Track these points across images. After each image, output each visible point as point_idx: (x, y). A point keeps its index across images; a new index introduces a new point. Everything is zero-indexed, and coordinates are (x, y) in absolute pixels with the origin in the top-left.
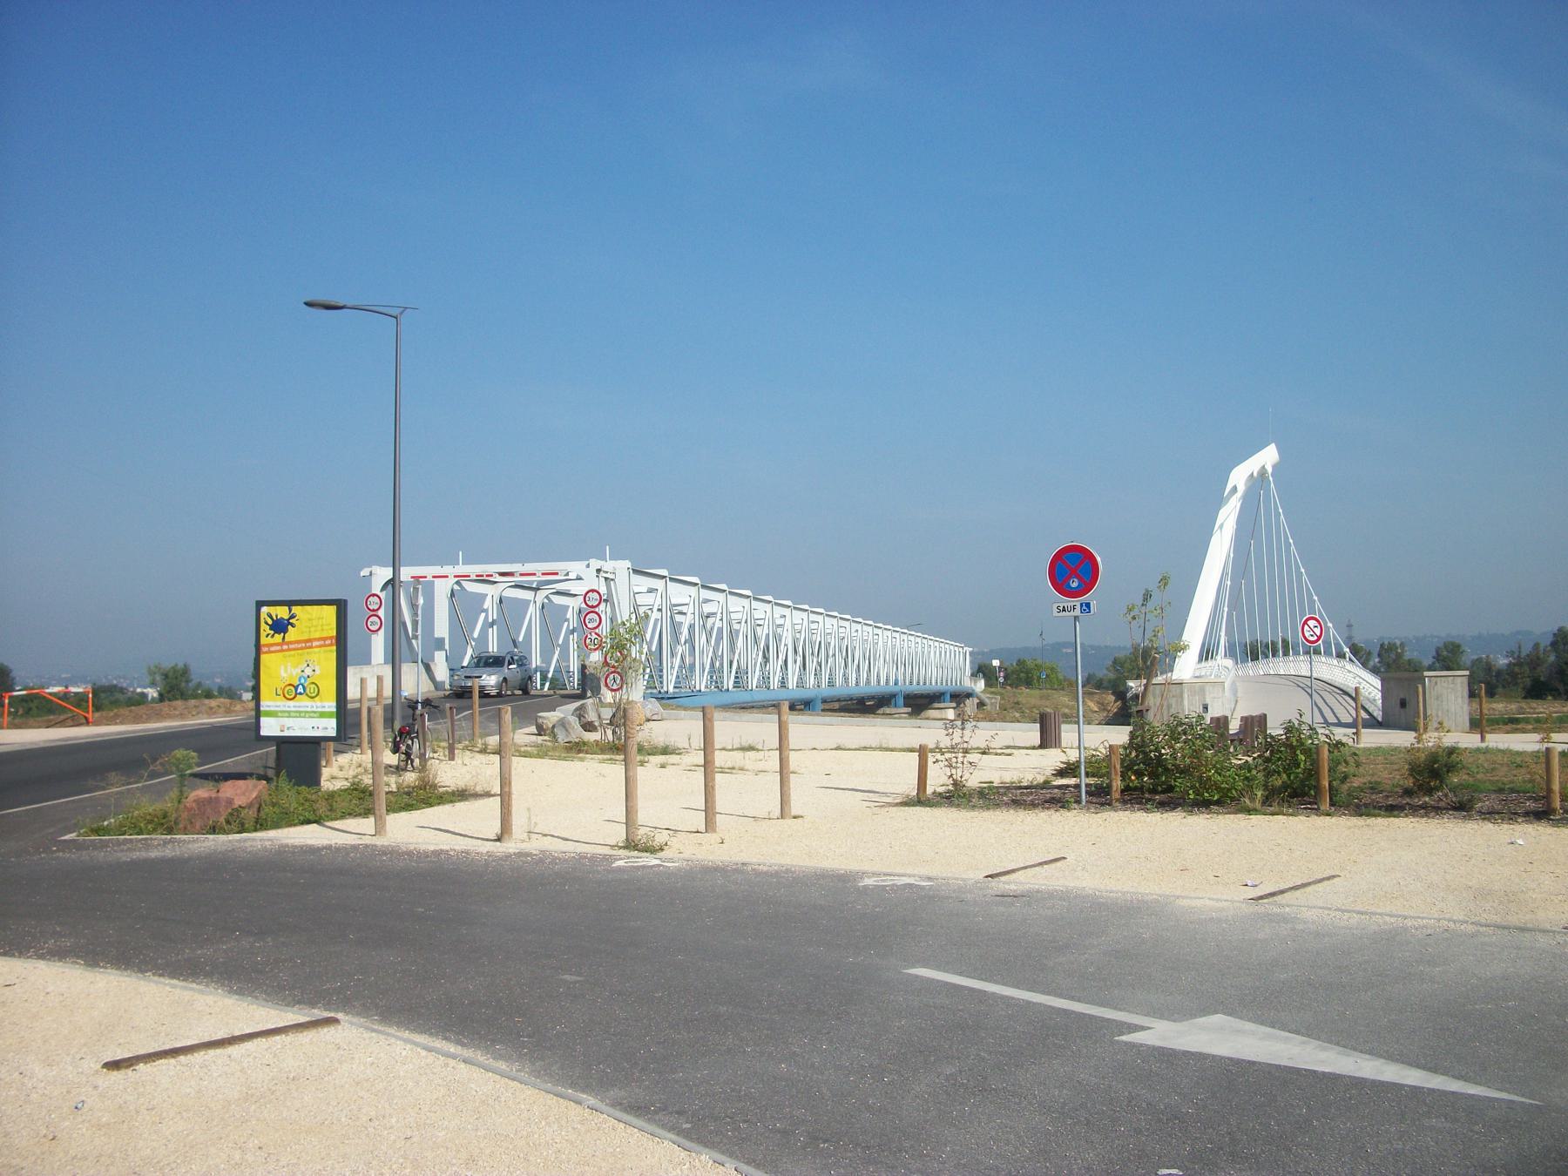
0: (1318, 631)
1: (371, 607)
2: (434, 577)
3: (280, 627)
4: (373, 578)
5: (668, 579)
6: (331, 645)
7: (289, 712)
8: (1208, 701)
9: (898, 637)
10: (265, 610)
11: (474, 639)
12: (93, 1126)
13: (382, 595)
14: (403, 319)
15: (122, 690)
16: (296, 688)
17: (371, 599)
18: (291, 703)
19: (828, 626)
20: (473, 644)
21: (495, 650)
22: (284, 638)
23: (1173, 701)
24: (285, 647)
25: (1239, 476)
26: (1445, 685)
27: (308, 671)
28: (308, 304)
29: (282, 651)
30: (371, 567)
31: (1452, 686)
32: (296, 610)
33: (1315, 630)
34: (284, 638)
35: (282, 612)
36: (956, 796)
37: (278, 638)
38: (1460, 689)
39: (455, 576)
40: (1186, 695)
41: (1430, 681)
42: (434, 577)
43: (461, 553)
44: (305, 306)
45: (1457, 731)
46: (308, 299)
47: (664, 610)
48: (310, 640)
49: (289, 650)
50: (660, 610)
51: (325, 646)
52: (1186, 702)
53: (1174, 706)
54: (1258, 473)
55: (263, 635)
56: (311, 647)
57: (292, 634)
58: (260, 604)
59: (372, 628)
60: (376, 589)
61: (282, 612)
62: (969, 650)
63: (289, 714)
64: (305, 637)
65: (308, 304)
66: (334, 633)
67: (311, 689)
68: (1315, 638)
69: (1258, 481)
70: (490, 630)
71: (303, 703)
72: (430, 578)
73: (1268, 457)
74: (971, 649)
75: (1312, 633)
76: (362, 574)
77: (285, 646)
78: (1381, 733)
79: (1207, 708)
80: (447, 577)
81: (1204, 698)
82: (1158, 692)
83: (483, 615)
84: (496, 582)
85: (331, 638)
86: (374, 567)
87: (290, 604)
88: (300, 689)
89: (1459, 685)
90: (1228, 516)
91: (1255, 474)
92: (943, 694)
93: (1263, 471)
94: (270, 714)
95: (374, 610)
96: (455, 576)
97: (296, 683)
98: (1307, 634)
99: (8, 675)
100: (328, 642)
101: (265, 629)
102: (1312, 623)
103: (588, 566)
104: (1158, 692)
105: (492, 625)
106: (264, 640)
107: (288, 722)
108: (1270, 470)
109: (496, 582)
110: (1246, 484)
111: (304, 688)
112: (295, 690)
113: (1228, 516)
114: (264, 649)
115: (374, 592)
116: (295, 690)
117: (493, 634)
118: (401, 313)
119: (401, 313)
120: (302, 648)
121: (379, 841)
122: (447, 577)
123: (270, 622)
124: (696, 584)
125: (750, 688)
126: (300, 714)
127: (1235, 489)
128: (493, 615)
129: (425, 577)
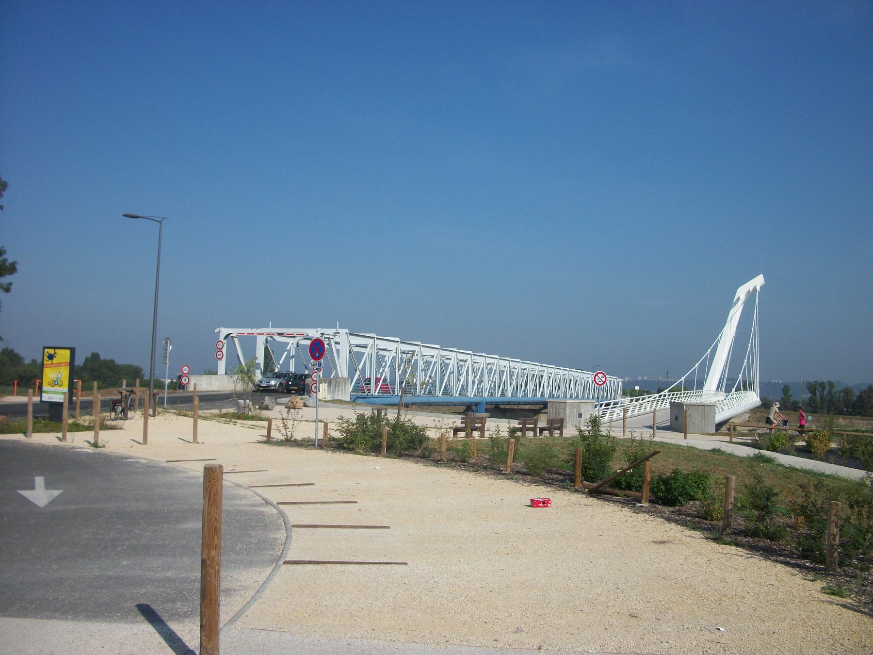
0: (603, 379)
1: (219, 347)
2: (258, 334)
3: (51, 357)
4: (221, 333)
5: (376, 339)
6: (68, 365)
7: (52, 392)
8: (582, 411)
9: (546, 370)
10: (46, 350)
11: (280, 365)
12: (78, 567)
13: (224, 342)
14: (163, 223)
15: (783, 389)
16: (55, 382)
17: (219, 343)
18: (53, 388)
19: (499, 363)
20: (279, 366)
21: (293, 371)
22: (52, 362)
23: (561, 411)
24: (52, 365)
25: (742, 293)
26: (694, 410)
27: (59, 376)
28: (125, 215)
29: (51, 367)
30: (219, 327)
31: (697, 410)
32: (57, 351)
33: (602, 379)
34: (52, 362)
35: (52, 351)
36: (289, 442)
37: (50, 362)
38: (701, 412)
39: (267, 334)
40: (568, 409)
41: (686, 407)
42: (258, 334)
43: (270, 322)
44: (123, 217)
45: (698, 433)
46: (124, 213)
47: (419, 355)
48: (60, 363)
49: (53, 367)
50: (417, 355)
51: (66, 366)
52: (568, 412)
53: (561, 413)
54: (752, 290)
55: (45, 360)
56: (61, 366)
57: (55, 360)
58: (45, 348)
59: (219, 357)
60: (222, 339)
61: (52, 351)
62: (620, 380)
63: (52, 392)
64: (59, 362)
65: (125, 215)
66: (69, 361)
67: (60, 383)
68: (602, 383)
69: (751, 295)
70: (291, 360)
71: (57, 388)
72: (255, 334)
73: (758, 281)
74: (623, 380)
75: (600, 380)
76: (216, 331)
77: (52, 365)
78: (660, 432)
79: (581, 415)
80: (263, 334)
81: (580, 410)
82: (554, 406)
83: (286, 353)
84: (295, 337)
85: (68, 363)
86: (221, 328)
87: (55, 348)
88: (56, 383)
89: (700, 410)
90: (735, 314)
91: (751, 290)
92: (477, 404)
93: (755, 289)
94: (46, 392)
95: (220, 349)
96: (267, 334)
97: (55, 380)
98: (597, 381)
99: (141, 372)
100: (66, 364)
101: (46, 358)
102: (600, 375)
103: (317, 332)
104: (554, 406)
105: (292, 358)
106: (45, 362)
107: (52, 395)
108: (758, 289)
109: (295, 337)
110: (745, 296)
111: (58, 382)
112: (55, 383)
113: (735, 314)
114: (45, 366)
115: (220, 340)
116: (55, 383)
117: (292, 362)
118: (162, 220)
119: (162, 220)
120: (58, 366)
121: (63, 444)
122: (263, 334)
123: (48, 355)
124: (398, 342)
125: (437, 395)
126: (56, 393)
127: (739, 298)
128: (293, 353)
129: (253, 334)
